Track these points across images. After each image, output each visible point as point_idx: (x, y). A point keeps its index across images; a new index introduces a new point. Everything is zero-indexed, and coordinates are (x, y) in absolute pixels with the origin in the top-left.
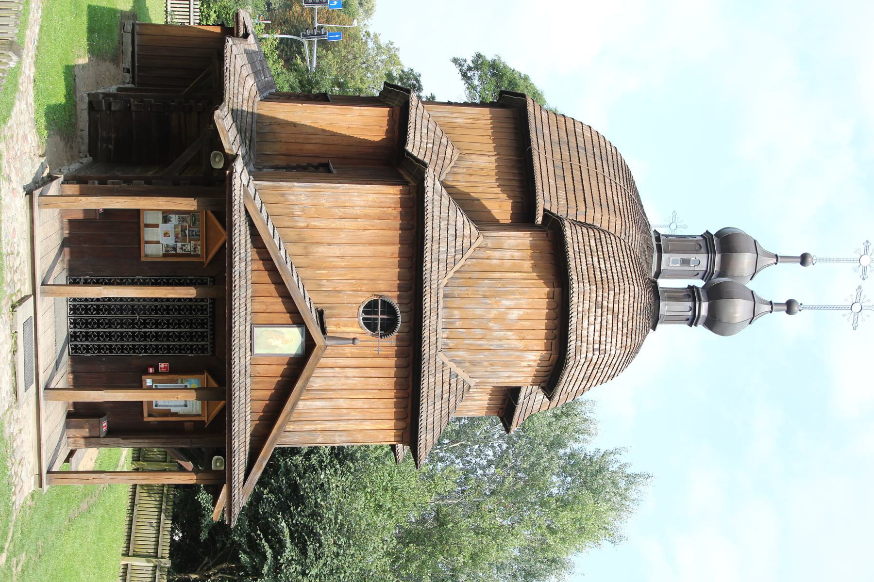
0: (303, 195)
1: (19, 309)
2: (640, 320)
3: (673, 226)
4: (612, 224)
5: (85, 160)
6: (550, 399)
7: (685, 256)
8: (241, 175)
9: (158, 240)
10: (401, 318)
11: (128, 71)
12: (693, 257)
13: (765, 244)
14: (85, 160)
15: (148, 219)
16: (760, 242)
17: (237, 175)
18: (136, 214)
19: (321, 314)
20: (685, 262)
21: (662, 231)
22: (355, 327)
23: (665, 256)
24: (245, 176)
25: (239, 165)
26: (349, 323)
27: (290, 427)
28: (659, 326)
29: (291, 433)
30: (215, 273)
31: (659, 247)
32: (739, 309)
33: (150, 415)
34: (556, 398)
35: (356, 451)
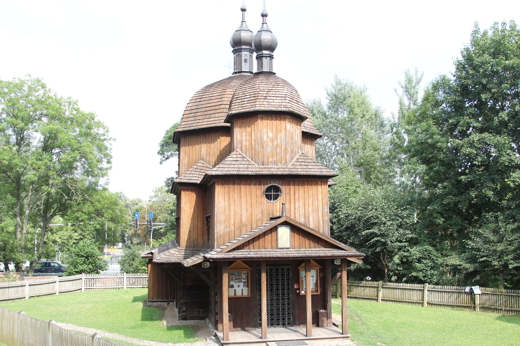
0: (220, 228)
2: (272, 79)
3: (230, 66)
6: (307, 118)
7: (243, 61)
8: (212, 255)
10: (273, 184)
11: (169, 303)
12: (243, 58)
13: (237, 27)
14: (208, 321)
15: (232, 294)
18: (230, 299)
19: (272, 219)
20: (246, 61)
23: (243, 70)
25: (208, 256)
26: (275, 207)
28: (274, 72)
29: (323, 229)
30: (254, 266)
31: (239, 72)
32: (266, 37)
33: (317, 292)
34: (306, 115)
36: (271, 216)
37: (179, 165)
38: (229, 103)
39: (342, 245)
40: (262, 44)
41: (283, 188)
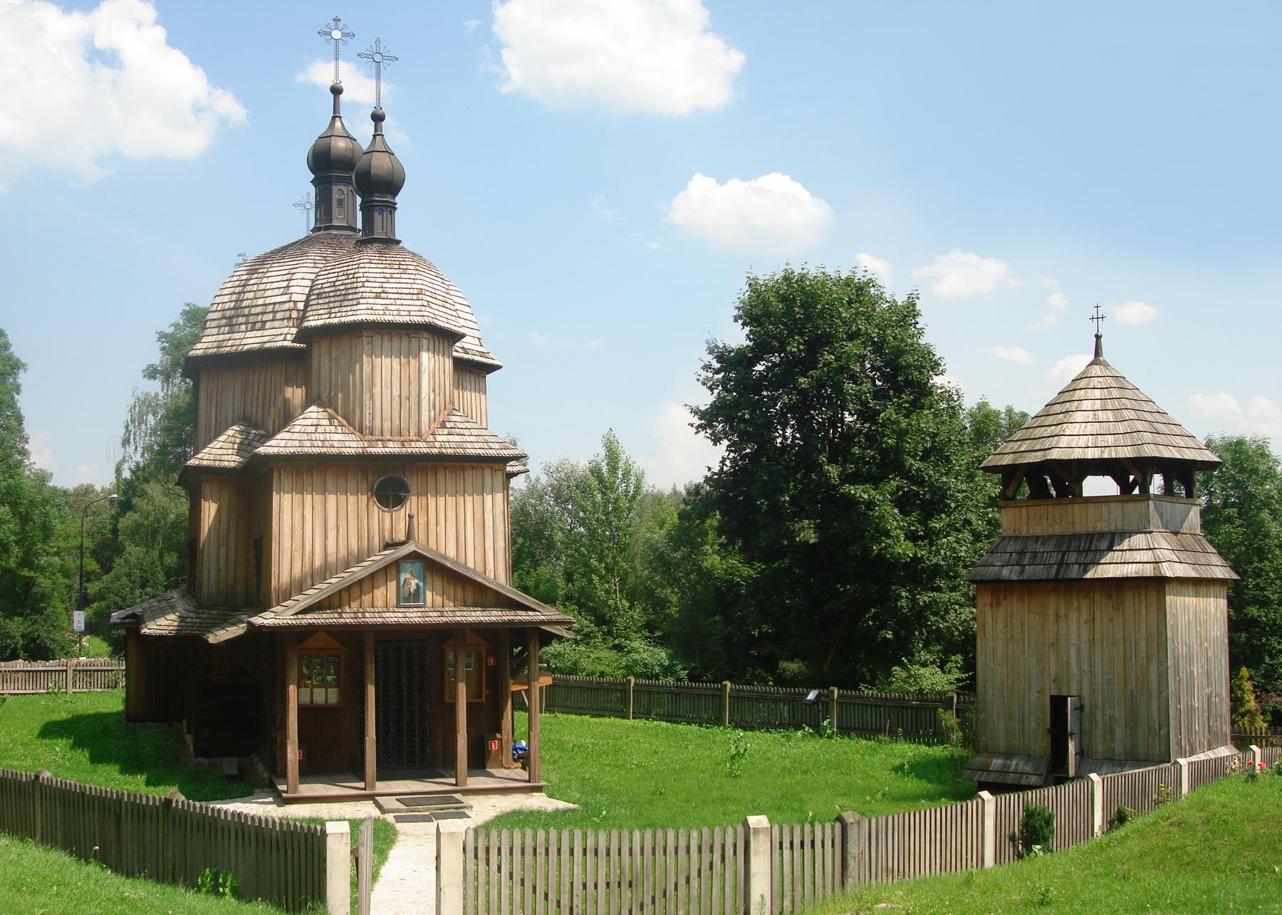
0: (287, 562)
1: (386, 807)
2: (392, 256)
3: (308, 206)
4: (307, 276)
5: (255, 760)
6: (463, 336)
7: (335, 203)
8: (266, 619)
9: (326, 696)
10: (390, 478)
11: (170, 726)
12: (335, 196)
13: (322, 129)
14: (255, 760)
15: (306, 700)
16: (320, 134)
17: (266, 622)
18: (301, 709)
19: (388, 546)
20: (340, 202)
21: (312, 225)
22: (401, 515)
23: (335, 223)
24: (267, 614)
25: (257, 620)
26: (394, 522)
27: (471, 565)
28: (397, 237)
29: (494, 567)
30: (354, 639)
31: (326, 228)
32: (379, 164)
33: (481, 697)
34: (462, 330)
35: (908, 352)
36: (388, 539)
37: (438, 868)
38: (304, 297)
39: (310, 619)
40: (373, 171)
41: (412, 482)
